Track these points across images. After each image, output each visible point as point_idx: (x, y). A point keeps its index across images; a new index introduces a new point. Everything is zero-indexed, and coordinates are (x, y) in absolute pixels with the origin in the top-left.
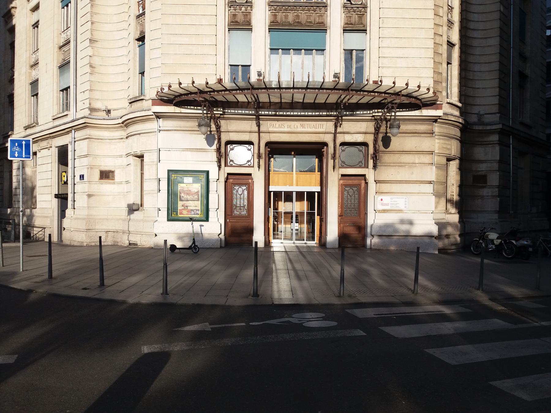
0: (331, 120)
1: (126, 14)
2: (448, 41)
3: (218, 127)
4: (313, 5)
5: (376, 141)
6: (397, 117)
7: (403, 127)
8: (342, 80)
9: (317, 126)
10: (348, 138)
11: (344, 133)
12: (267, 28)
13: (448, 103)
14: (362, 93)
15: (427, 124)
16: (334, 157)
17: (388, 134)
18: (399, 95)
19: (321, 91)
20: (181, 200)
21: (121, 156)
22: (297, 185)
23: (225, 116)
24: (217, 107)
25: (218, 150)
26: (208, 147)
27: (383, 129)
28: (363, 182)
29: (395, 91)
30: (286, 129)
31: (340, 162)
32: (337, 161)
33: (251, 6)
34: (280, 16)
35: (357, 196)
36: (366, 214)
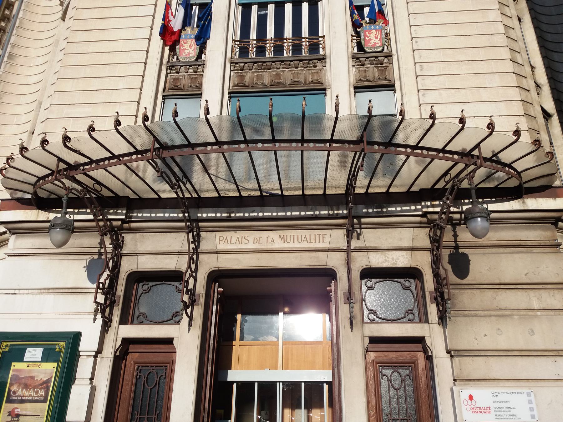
0: (338, 227)
5: (436, 262)
9: (312, 237)
10: (378, 260)
11: (367, 250)
15: (540, 228)
17: (461, 251)
20: (9, 401)
22: (286, 367)
23: (133, 225)
27: (447, 238)
28: (421, 356)
34: (249, 77)
35: (410, 390)
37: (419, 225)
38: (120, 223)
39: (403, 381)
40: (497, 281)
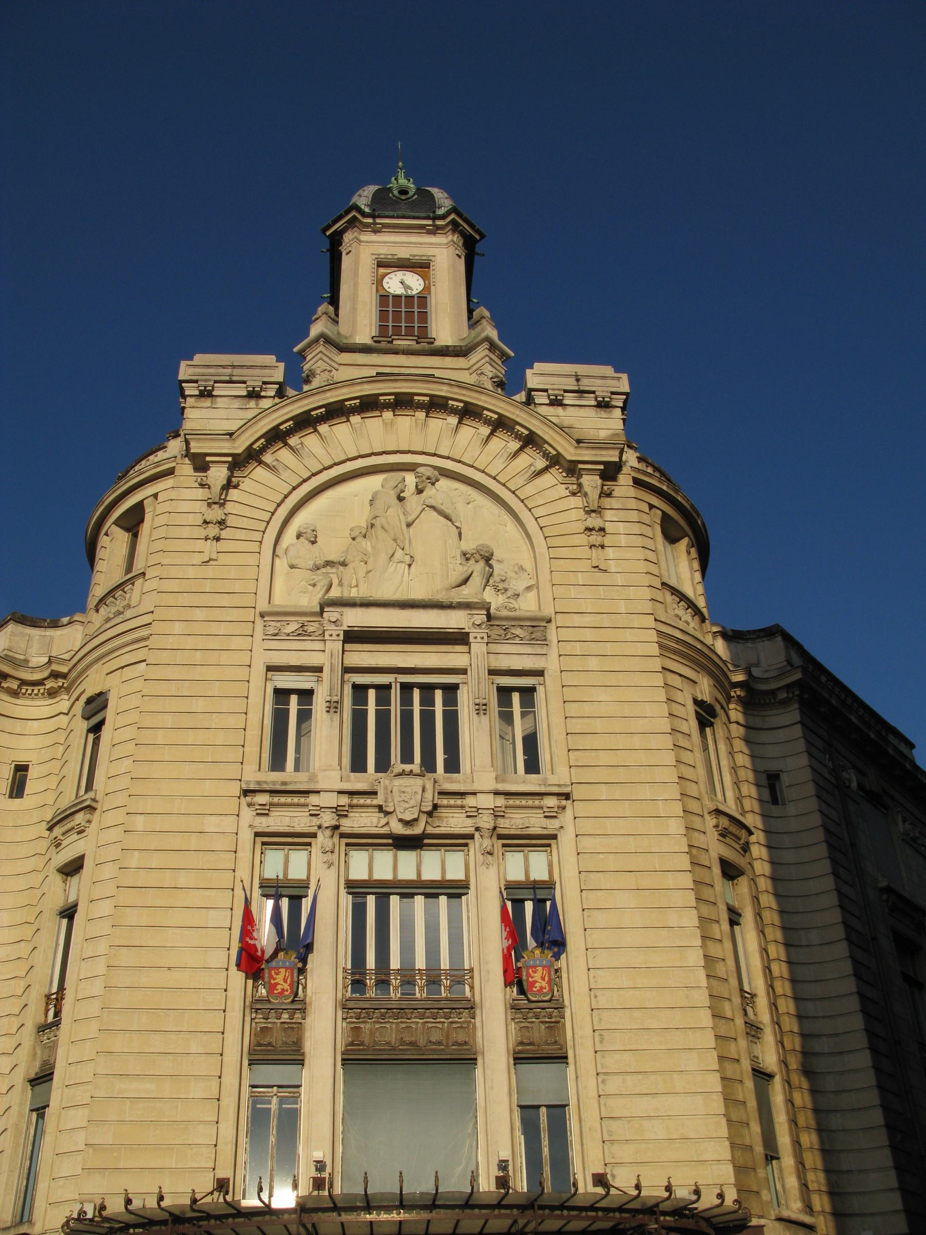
1: (13, 1019)
2: (753, 1070)
4: (442, 1004)
8: (521, 1184)
12: (339, 1059)
13: (780, 1219)
14: (565, 1212)
19: (468, 1211)
33: (303, 1010)
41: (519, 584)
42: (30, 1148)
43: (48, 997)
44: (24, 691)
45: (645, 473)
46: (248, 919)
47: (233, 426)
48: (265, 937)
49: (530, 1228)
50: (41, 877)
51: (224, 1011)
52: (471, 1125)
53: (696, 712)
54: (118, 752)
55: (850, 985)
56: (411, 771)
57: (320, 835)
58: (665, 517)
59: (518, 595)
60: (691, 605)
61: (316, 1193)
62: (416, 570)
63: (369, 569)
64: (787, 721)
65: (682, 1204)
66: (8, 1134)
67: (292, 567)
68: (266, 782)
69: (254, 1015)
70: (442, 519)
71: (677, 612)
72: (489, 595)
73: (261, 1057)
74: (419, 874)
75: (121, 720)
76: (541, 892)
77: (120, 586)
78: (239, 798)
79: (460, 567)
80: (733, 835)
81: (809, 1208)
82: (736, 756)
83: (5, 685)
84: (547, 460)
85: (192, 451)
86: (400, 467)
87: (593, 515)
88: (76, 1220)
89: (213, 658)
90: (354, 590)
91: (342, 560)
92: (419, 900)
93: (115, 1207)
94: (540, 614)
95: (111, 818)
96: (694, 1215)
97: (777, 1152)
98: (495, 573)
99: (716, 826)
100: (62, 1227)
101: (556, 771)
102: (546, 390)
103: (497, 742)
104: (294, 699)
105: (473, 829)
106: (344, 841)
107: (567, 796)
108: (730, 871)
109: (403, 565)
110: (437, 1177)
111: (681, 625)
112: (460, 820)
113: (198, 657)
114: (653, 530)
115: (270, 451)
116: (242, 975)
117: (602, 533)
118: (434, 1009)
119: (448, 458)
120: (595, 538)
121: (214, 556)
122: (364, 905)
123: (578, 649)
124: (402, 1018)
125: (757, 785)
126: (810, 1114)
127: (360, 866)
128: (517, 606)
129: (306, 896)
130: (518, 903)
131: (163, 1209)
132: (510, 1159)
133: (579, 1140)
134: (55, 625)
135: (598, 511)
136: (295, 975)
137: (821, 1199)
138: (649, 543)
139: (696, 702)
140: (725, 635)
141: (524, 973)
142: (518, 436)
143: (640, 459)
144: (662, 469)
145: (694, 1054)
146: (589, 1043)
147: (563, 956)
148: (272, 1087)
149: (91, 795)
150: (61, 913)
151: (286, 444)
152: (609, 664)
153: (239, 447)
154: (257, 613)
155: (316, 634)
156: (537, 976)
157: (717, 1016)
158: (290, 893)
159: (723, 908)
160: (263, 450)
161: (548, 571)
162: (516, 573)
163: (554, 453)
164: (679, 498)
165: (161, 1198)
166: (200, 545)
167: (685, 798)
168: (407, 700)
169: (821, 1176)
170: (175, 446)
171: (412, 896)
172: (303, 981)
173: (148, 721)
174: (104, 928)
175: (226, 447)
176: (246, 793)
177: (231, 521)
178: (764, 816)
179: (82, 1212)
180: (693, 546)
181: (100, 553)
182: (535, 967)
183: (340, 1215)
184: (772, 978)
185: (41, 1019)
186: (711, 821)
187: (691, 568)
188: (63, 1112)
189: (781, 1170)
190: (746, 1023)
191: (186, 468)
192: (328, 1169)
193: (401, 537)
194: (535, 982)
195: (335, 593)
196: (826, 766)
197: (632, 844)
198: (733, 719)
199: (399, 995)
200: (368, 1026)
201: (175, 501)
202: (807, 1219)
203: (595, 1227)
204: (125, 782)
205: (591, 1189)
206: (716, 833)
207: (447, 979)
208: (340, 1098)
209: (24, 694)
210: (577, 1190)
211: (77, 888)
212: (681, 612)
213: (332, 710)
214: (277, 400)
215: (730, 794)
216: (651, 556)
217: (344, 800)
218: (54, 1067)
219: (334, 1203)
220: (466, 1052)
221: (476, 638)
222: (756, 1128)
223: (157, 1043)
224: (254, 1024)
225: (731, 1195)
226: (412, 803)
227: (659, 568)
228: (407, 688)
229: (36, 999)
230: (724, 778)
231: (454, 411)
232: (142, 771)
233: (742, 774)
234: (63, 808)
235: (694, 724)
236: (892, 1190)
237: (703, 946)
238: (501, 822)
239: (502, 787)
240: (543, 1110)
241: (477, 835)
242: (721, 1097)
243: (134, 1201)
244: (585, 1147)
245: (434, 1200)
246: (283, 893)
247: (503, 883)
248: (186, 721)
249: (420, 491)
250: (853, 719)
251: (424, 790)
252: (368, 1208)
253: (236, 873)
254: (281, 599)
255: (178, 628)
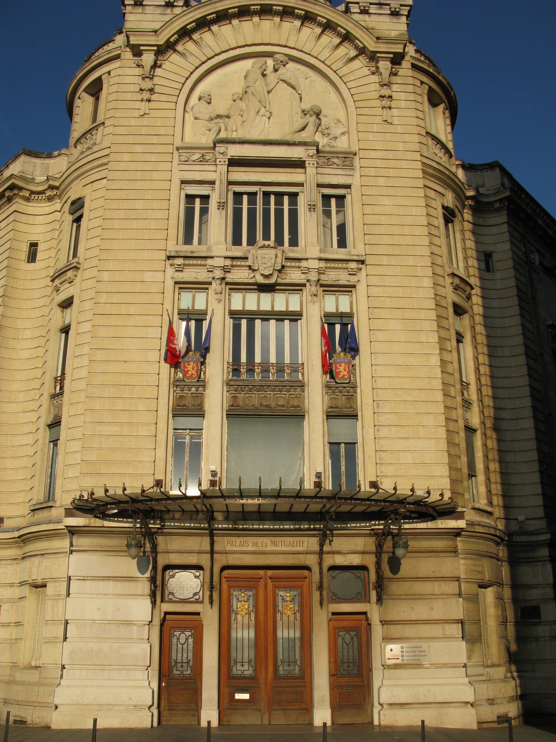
0: (313, 536)
1: (37, 391)
2: (465, 426)
3: (154, 547)
5: (378, 564)
6: (402, 531)
7: (413, 544)
8: (328, 485)
9: (295, 543)
10: (340, 560)
13: (474, 509)
14: (353, 501)
16: (320, 587)
18: (404, 503)
19: (297, 499)
21: (12, 585)
23: (165, 531)
24: (154, 518)
25: (153, 579)
26: (139, 575)
29: (397, 498)
30: (250, 548)
31: (330, 593)
32: (325, 593)
33: (204, 386)
35: (356, 644)
36: (371, 670)
37: (370, 535)
38: (156, 530)
39: (352, 639)
40: (415, 576)
41: (336, 131)
42: (50, 462)
43: (56, 379)
44: (33, 198)
45: (419, 60)
46: (171, 333)
47: (157, 26)
48: (181, 342)
49: (332, 510)
50: (48, 309)
51: (158, 386)
52: (301, 453)
53: (444, 214)
54: (92, 234)
55: (525, 380)
56: (269, 245)
57: (213, 283)
58: (431, 89)
59: (336, 138)
60: (444, 147)
61: (212, 488)
62: (273, 121)
63: (244, 120)
64: (499, 221)
65: (419, 499)
66: (38, 453)
67: (196, 118)
68: (181, 251)
69: (175, 389)
70: (290, 88)
71: (435, 151)
72: (318, 138)
73: (180, 413)
74: (273, 307)
75: (93, 215)
76: (345, 319)
77: (89, 131)
78: (165, 261)
79: (301, 120)
80: (462, 289)
81: (490, 503)
82: (466, 241)
83: (21, 194)
84: (357, 50)
85: (131, 43)
86: (263, 55)
87: (385, 87)
88: (79, 500)
89: (148, 175)
90: (234, 134)
91: (227, 114)
92: (273, 323)
93: (99, 493)
94: (349, 150)
95: (88, 274)
96: (426, 505)
97: (475, 472)
98: (323, 123)
99: (452, 283)
100: (71, 503)
101: (356, 247)
102: (358, 3)
103: (321, 228)
104: (198, 201)
105: (306, 280)
106: (228, 287)
107: (363, 262)
108: (459, 311)
109: (265, 118)
110: (280, 480)
111: (437, 159)
112: (298, 275)
113: (139, 175)
114: (423, 98)
115: (181, 43)
116: (167, 366)
117: (390, 99)
118: (280, 386)
119: (294, 48)
120: (386, 102)
121: (147, 112)
122: (240, 325)
123: (372, 172)
124: (261, 391)
125: (478, 260)
126: (496, 453)
127: (237, 301)
128: (335, 145)
129: (206, 319)
130: (332, 325)
131: (126, 495)
132: (323, 472)
133: (362, 463)
134: (50, 156)
135: (388, 85)
136: (199, 365)
137: (498, 499)
138: (419, 107)
139: (444, 207)
140: (463, 167)
141: (334, 367)
142: (339, 35)
143: (417, 51)
144: (431, 58)
145: (431, 416)
146: (371, 408)
147: (357, 357)
148: (186, 429)
149: (76, 260)
150: (61, 330)
151: (191, 38)
152: (391, 182)
153: (162, 39)
154: (175, 147)
155: (211, 161)
156: (341, 369)
157: (446, 395)
158: (197, 317)
159: (453, 332)
160: (176, 42)
161: (355, 123)
162: (335, 124)
163: (362, 46)
164: (440, 78)
165: (125, 489)
166: (138, 105)
167: (434, 266)
168: (266, 202)
169: (499, 487)
170: (120, 40)
171: (268, 320)
172: (204, 369)
173: (109, 215)
174: (87, 338)
175: (153, 40)
176: (169, 258)
177: (157, 89)
178: (481, 278)
179: (81, 496)
180: (447, 109)
181: (76, 111)
182: (340, 363)
183: (225, 500)
184: (480, 375)
185: (52, 391)
186: (449, 280)
187: (445, 123)
188: (68, 442)
189: (476, 483)
190: (463, 400)
191: (128, 55)
192: (219, 475)
193: (264, 100)
194: (340, 372)
195: (223, 135)
196: (520, 250)
197: (400, 292)
198: (465, 219)
199: (260, 378)
200: (242, 395)
201: (122, 76)
202: (489, 509)
203: (369, 510)
204: (96, 252)
205: (368, 489)
206: (451, 288)
207: (288, 369)
208: (225, 436)
209: (33, 199)
210: (360, 489)
211: (70, 315)
212: (437, 151)
213: (221, 208)
214: (185, 8)
215: (461, 265)
216: (420, 115)
217: (228, 262)
218: (61, 418)
219: (222, 493)
220: (299, 411)
221: (309, 164)
222: (464, 459)
223: (119, 405)
224: (175, 394)
225: (447, 495)
226: (269, 264)
227: (425, 123)
228: (266, 195)
229: (49, 380)
230: (458, 255)
231: (298, 17)
232: (106, 245)
233: (469, 253)
234: (59, 268)
235: (441, 221)
236: (538, 495)
237: (440, 354)
238: (323, 277)
239: (323, 256)
240: (343, 445)
241: (308, 284)
242: (446, 441)
243: (110, 491)
244: (366, 466)
245: (279, 493)
246: (192, 318)
247: (323, 313)
248: (132, 214)
249: (276, 70)
250: (540, 222)
251: (276, 257)
252: (241, 497)
253: (164, 306)
254: (189, 139)
255: (126, 157)
